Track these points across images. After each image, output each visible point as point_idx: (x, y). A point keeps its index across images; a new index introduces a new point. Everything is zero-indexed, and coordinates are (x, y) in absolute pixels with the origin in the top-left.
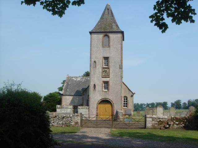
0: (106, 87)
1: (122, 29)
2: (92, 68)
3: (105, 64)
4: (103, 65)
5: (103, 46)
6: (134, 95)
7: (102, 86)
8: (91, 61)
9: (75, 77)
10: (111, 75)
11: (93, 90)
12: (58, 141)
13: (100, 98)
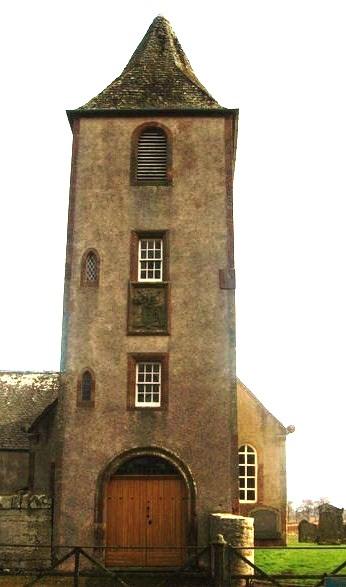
0: (151, 265)
1: (225, 102)
2: (74, 288)
3: (143, 267)
4: (133, 272)
5: (137, 180)
6: (289, 437)
7: (131, 384)
8: (70, 250)
9: (10, 373)
10: (177, 323)
11: (78, 404)
12: (187, 521)
13: (119, 448)
